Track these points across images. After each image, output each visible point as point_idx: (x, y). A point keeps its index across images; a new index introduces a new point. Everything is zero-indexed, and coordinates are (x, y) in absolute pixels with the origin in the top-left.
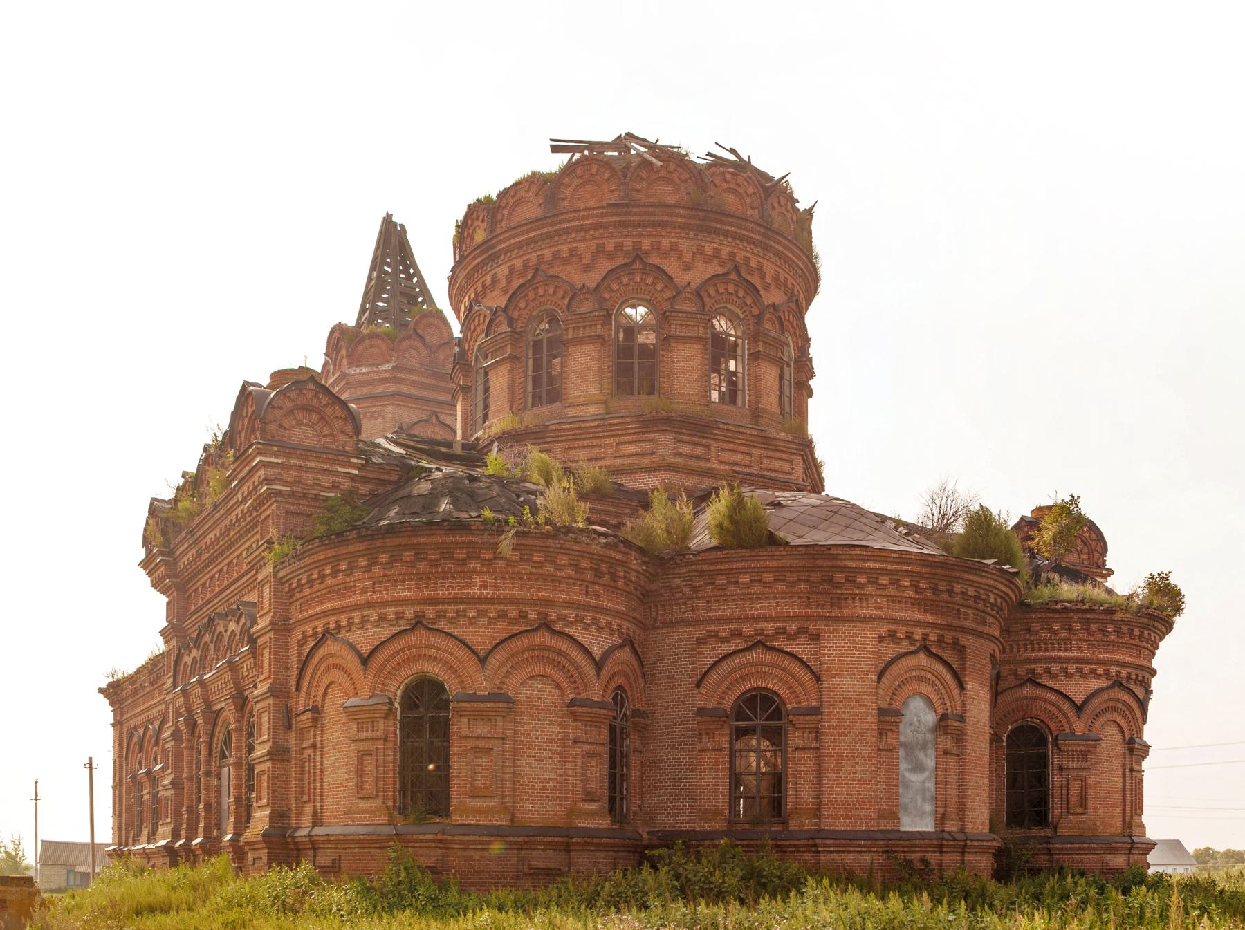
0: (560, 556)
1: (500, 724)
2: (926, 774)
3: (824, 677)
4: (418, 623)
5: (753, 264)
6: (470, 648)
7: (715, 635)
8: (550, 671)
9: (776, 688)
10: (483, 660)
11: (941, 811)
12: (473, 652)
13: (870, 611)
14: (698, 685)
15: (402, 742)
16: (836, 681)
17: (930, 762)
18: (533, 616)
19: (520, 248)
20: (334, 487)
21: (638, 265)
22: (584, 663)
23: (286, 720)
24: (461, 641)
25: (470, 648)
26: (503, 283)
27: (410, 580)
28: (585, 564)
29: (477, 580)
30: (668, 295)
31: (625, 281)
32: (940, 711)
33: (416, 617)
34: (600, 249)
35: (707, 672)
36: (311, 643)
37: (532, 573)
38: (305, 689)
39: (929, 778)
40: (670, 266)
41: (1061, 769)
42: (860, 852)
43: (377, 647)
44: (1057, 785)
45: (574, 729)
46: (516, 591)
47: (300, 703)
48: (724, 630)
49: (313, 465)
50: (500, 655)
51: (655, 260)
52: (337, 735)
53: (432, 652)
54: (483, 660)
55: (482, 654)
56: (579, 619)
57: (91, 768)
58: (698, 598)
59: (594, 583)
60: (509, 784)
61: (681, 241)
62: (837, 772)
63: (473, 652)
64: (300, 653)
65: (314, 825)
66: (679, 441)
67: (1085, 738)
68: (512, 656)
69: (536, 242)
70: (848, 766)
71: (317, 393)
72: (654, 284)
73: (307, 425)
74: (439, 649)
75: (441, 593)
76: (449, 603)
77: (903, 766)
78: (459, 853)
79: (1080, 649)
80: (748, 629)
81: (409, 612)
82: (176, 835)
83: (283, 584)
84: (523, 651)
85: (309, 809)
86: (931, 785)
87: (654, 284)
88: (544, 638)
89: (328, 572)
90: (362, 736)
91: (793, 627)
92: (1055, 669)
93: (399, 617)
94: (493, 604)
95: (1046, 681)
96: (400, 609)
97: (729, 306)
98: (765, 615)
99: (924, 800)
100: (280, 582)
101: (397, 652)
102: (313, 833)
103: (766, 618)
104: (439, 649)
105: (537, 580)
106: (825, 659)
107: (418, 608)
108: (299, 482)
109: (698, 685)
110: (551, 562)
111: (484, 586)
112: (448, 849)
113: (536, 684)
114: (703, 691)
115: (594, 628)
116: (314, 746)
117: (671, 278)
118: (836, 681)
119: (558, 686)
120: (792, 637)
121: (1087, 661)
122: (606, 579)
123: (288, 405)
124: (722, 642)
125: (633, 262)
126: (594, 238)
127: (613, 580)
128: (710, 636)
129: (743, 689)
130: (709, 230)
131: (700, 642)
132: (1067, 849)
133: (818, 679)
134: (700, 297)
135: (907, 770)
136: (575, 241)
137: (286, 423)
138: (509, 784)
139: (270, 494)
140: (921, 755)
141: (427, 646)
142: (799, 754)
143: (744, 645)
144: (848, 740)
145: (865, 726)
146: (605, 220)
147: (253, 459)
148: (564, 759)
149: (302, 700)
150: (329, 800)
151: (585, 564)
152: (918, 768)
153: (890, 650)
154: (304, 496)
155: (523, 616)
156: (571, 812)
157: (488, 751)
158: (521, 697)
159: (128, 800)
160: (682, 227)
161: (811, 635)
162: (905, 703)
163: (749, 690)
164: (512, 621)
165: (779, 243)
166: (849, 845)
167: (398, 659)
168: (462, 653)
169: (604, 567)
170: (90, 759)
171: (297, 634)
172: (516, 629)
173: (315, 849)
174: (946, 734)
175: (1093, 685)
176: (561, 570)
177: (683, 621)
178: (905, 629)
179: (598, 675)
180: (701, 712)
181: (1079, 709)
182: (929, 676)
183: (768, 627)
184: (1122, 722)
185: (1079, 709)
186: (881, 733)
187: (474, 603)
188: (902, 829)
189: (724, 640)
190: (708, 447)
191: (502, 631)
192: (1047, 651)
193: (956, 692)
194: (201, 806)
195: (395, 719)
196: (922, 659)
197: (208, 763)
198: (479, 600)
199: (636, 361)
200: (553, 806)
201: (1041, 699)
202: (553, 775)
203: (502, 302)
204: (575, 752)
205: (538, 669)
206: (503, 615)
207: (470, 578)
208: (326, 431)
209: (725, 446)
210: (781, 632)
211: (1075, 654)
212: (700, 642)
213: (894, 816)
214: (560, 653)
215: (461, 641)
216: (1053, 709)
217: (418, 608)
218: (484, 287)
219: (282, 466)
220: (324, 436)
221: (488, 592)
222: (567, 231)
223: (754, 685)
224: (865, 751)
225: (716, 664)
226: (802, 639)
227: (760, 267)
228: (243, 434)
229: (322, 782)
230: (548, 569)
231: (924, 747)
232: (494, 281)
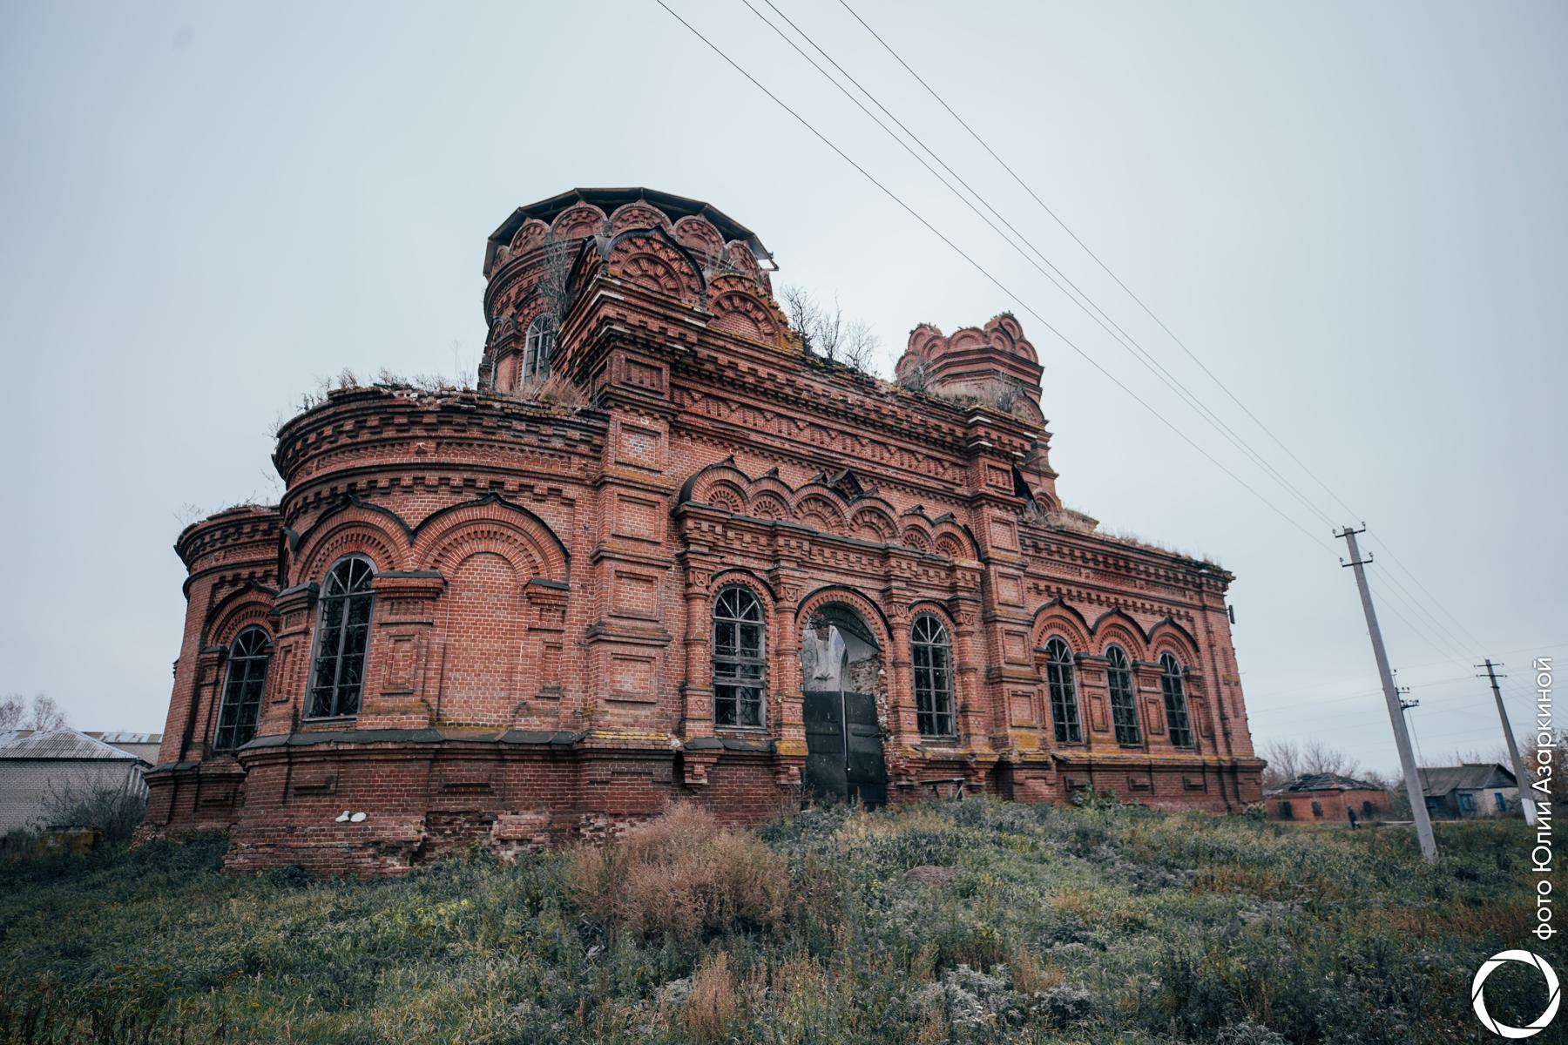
95: (375, 500)
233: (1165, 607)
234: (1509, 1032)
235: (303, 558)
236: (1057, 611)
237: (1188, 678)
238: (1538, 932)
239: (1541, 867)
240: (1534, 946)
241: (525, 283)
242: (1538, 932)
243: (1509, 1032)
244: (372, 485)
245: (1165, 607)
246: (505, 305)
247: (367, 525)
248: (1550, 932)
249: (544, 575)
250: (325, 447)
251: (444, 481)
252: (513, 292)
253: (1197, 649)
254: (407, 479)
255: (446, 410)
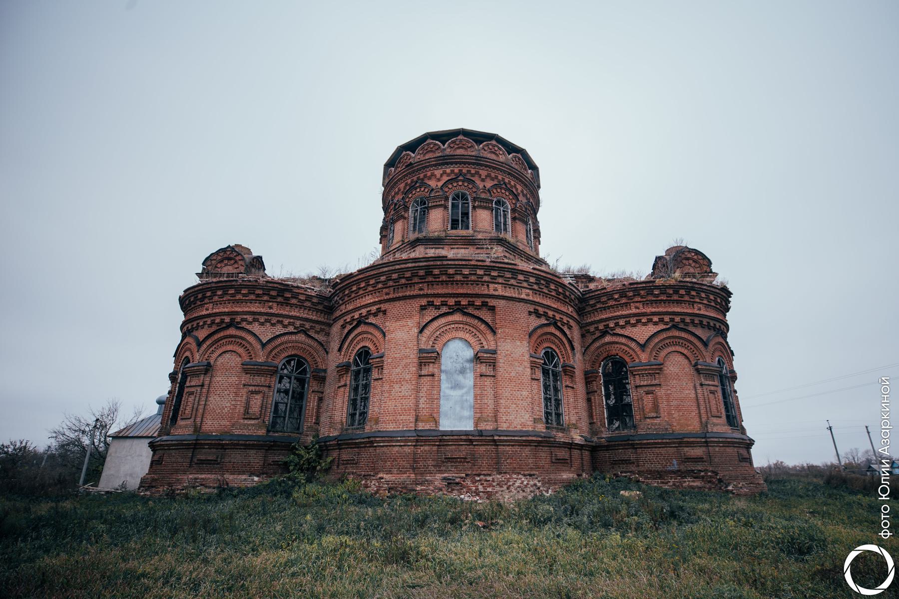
2: (464, 390)
13: (416, 292)
32: (478, 348)
42: (400, 446)
62: (390, 392)
70: (397, 387)
79: (637, 308)
95: (618, 331)
99: (462, 408)
113: (228, 355)
121: (644, 314)
130: (447, 164)
132: (645, 444)
135: (448, 388)
140: (460, 378)
142: (376, 383)
144: (398, 370)
145: (408, 361)
148: (236, 394)
152: (457, 386)
160: (435, 165)
166: (391, 441)
175: (652, 329)
181: (643, 347)
188: (441, 429)
200: (225, 423)
202: (228, 405)
204: (244, 391)
213: (437, 422)
216: (625, 348)
224: (408, 377)
227: (515, 186)
231: (462, 371)
233: (551, 313)
234: (865, 592)
235: (201, 352)
236: (552, 329)
237: (315, 378)
238: (882, 534)
239: (884, 497)
240: (880, 543)
241: (409, 181)
242: (882, 534)
243: (865, 592)
244: (617, 324)
245: (551, 313)
246: (397, 193)
247: (371, 334)
248: (889, 534)
249: (486, 347)
250: (353, 295)
251: (650, 321)
252: (402, 186)
253: (573, 348)
254: (633, 321)
255: (623, 293)
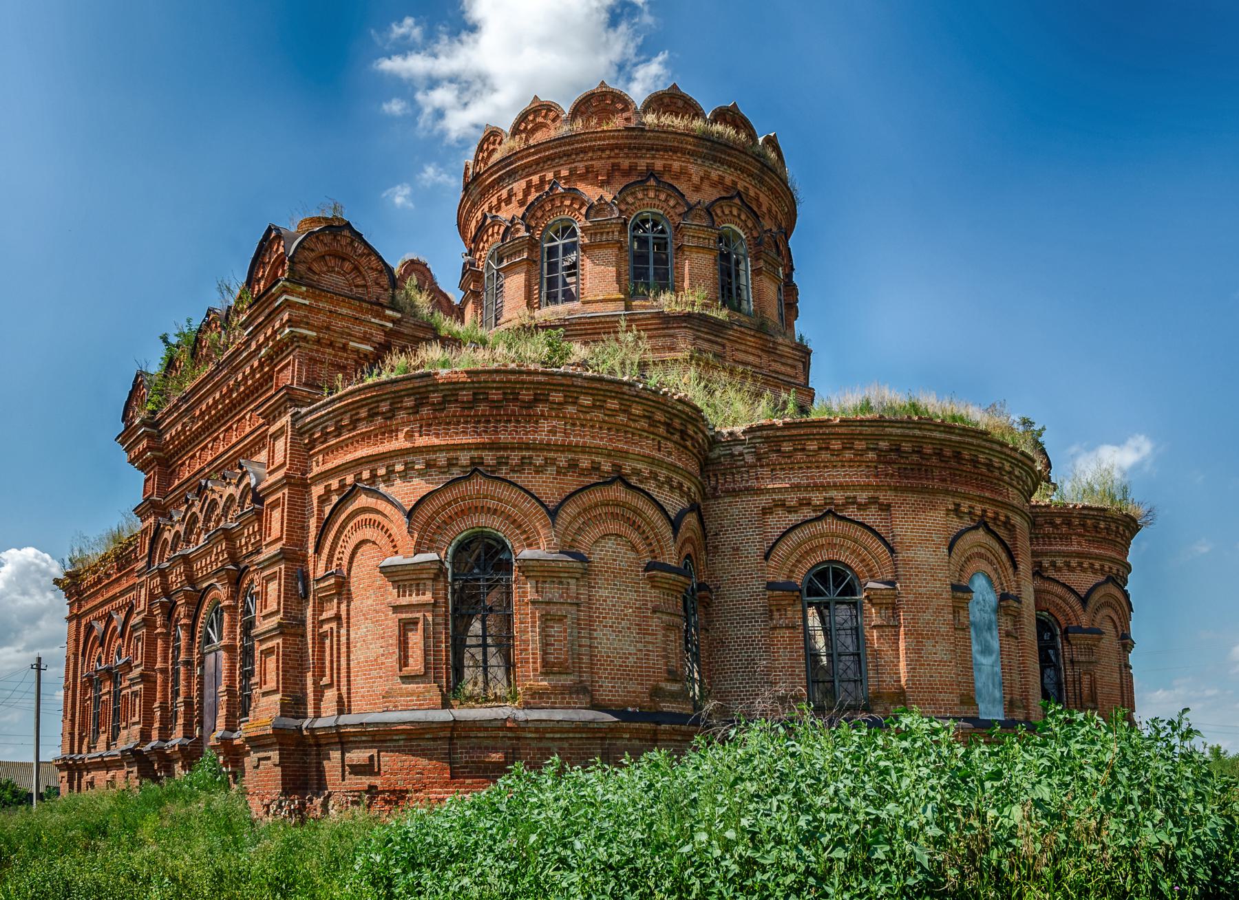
0: (634, 405)
1: (573, 587)
2: (994, 656)
3: (898, 549)
4: (475, 469)
5: (752, 193)
6: (537, 499)
7: (782, 504)
8: (625, 529)
9: (848, 561)
10: (553, 514)
11: (1008, 697)
12: (542, 504)
14: (766, 557)
15: (455, 610)
16: (911, 554)
17: (995, 645)
18: (607, 467)
19: (538, 164)
20: (365, 339)
21: (652, 182)
22: (660, 523)
23: (298, 587)
24: (527, 492)
25: (537, 499)
26: (520, 196)
27: (466, 422)
28: (659, 416)
29: (545, 425)
30: (680, 210)
31: (640, 195)
33: (473, 464)
34: (615, 168)
35: (774, 544)
36: (335, 499)
37: (604, 421)
38: (326, 550)
39: (996, 661)
40: (682, 187)
41: (1072, 662)
43: (423, 498)
44: (1070, 679)
45: (653, 595)
46: (588, 440)
47: (318, 568)
48: (792, 499)
49: (344, 311)
50: (571, 510)
51: (667, 178)
52: (370, 602)
53: (492, 504)
54: (553, 514)
55: (551, 506)
56: (654, 475)
57: (39, 669)
58: (762, 466)
59: (666, 439)
60: (585, 659)
61: (690, 166)
63: (542, 504)
64: (321, 511)
65: (340, 712)
66: (698, 338)
67: (1090, 631)
68: (585, 510)
69: (553, 160)
71: (352, 241)
72: (666, 201)
73: (339, 273)
74: (500, 500)
75: (503, 437)
76: (513, 449)
77: (975, 648)
78: (534, 744)
80: (817, 498)
81: (464, 458)
82: (145, 736)
83: (301, 435)
84: (596, 505)
85: (330, 694)
86: (998, 669)
87: (666, 201)
88: (617, 493)
89: (363, 415)
90: (404, 601)
91: (863, 497)
92: (1060, 562)
93: (451, 463)
94: (563, 452)
95: (1052, 574)
96: (452, 454)
97: (733, 226)
98: (835, 483)
100: (299, 433)
101: (449, 504)
102: (340, 723)
103: (835, 486)
104: (500, 500)
105: (609, 429)
106: (897, 531)
107: (475, 454)
108: (328, 328)
109: (766, 557)
110: (625, 411)
111: (553, 432)
112: (518, 738)
113: (610, 544)
114: (772, 564)
115: (666, 487)
116: (338, 618)
117: (683, 196)
118: (911, 554)
119: (634, 548)
120: (862, 507)
122: (676, 437)
123: (321, 249)
124: (789, 512)
125: (648, 179)
126: (609, 157)
127: (682, 438)
128: (776, 506)
129: (813, 562)
131: (766, 511)
133: (892, 551)
134: (710, 214)
136: (592, 159)
137: (316, 267)
138: (585, 659)
139: (293, 338)
141: (485, 497)
143: (813, 515)
146: (620, 141)
147: (276, 300)
148: (643, 631)
149: (322, 565)
150: (358, 682)
151: (659, 416)
152: (986, 651)
153: (956, 524)
154: (331, 345)
155: (596, 468)
156: (656, 692)
157: (561, 619)
158: (595, 558)
159: (83, 701)
160: (692, 154)
161: (882, 504)
162: (971, 580)
163: (818, 564)
164: (583, 473)
165: (772, 179)
167: (450, 511)
168: (528, 505)
169: (677, 423)
170: (39, 659)
171: (317, 491)
172: (587, 481)
173: (342, 743)
174: (1007, 614)
176: (634, 421)
177: (747, 489)
178: (968, 503)
179: (675, 537)
180: (771, 586)
182: (989, 555)
183: (838, 496)
184: (1115, 618)
185: (1084, 601)
186: (955, 611)
187: (542, 450)
189: (791, 510)
190: (724, 346)
191: (571, 482)
192: (1051, 545)
193: (1010, 571)
194: (180, 699)
195: (446, 581)
196: (980, 535)
197: (190, 650)
198: (548, 447)
199: (651, 267)
200: (633, 686)
201: (1049, 592)
202: (632, 650)
203: (520, 212)
205: (613, 527)
206: (573, 465)
207: (537, 422)
208: (359, 281)
209: (737, 346)
210: (852, 501)
211: (1075, 548)
212: (766, 511)
214: (636, 511)
215: (527, 492)
217: (475, 454)
218: (499, 200)
219: (310, 308)
220: (357, 286)
221: (559, 438)
222: (584, 151)
223: (825, 558)
225: (784, 534)
226: (873, 509)
228: (262, 283)
229: (348, 660)
230: (622, 418)
232: (511, 194)
